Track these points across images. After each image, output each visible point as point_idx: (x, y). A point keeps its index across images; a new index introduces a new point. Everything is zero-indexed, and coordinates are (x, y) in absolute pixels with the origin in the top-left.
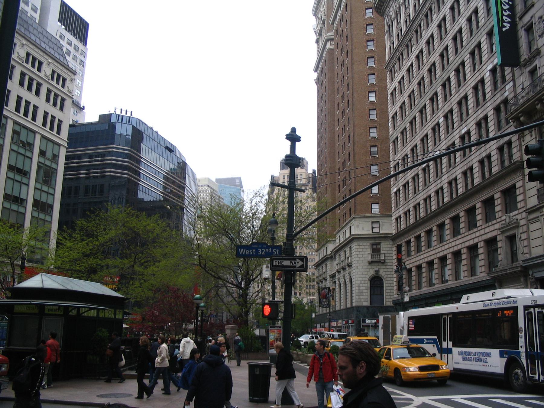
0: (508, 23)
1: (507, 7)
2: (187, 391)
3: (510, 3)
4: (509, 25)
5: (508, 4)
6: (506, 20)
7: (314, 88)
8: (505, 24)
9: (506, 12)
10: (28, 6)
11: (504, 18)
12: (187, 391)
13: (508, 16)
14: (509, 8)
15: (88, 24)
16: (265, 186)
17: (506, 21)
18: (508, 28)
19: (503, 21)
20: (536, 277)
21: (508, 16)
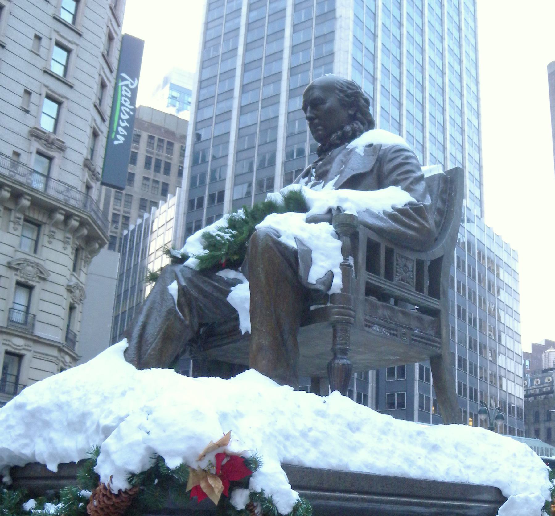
0: (123, 136)
1: (127, 117)
2: (544, 344)
3: (132, 113)
4: (123, 139)
5: (128, 113)
6: (122, 132)
7: (238, 376)
8: (119, 137)
9: (123, 122)
10: (287, 467)
11: (120, 129)
12: (544, 344)
13: (125, 128)
14: (128, 119)
15: (548, 66)
16: (157, 397)
17: (121, 133)
18: (121, 142)
19: (117, 133)
20: (105, 250)
21: (125, 128)
